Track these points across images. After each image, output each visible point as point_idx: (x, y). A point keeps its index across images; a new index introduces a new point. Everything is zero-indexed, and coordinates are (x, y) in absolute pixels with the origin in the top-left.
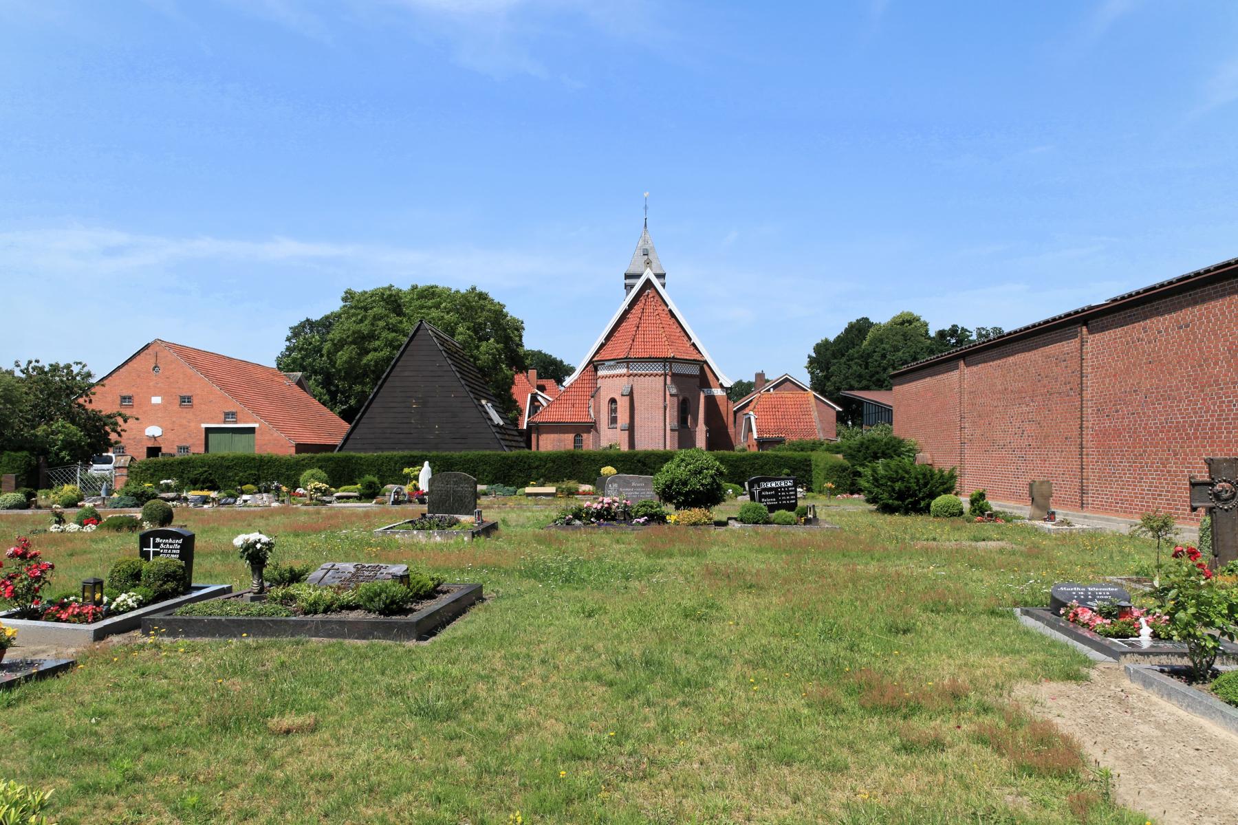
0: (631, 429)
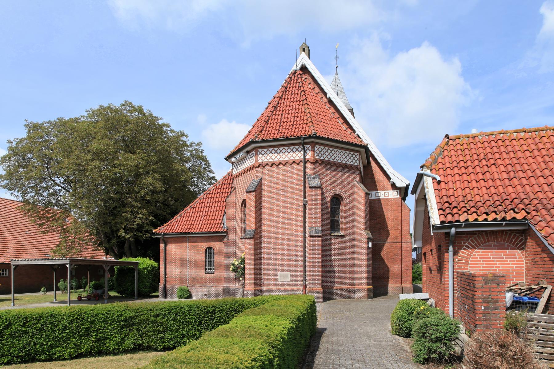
0: (257, 237)
